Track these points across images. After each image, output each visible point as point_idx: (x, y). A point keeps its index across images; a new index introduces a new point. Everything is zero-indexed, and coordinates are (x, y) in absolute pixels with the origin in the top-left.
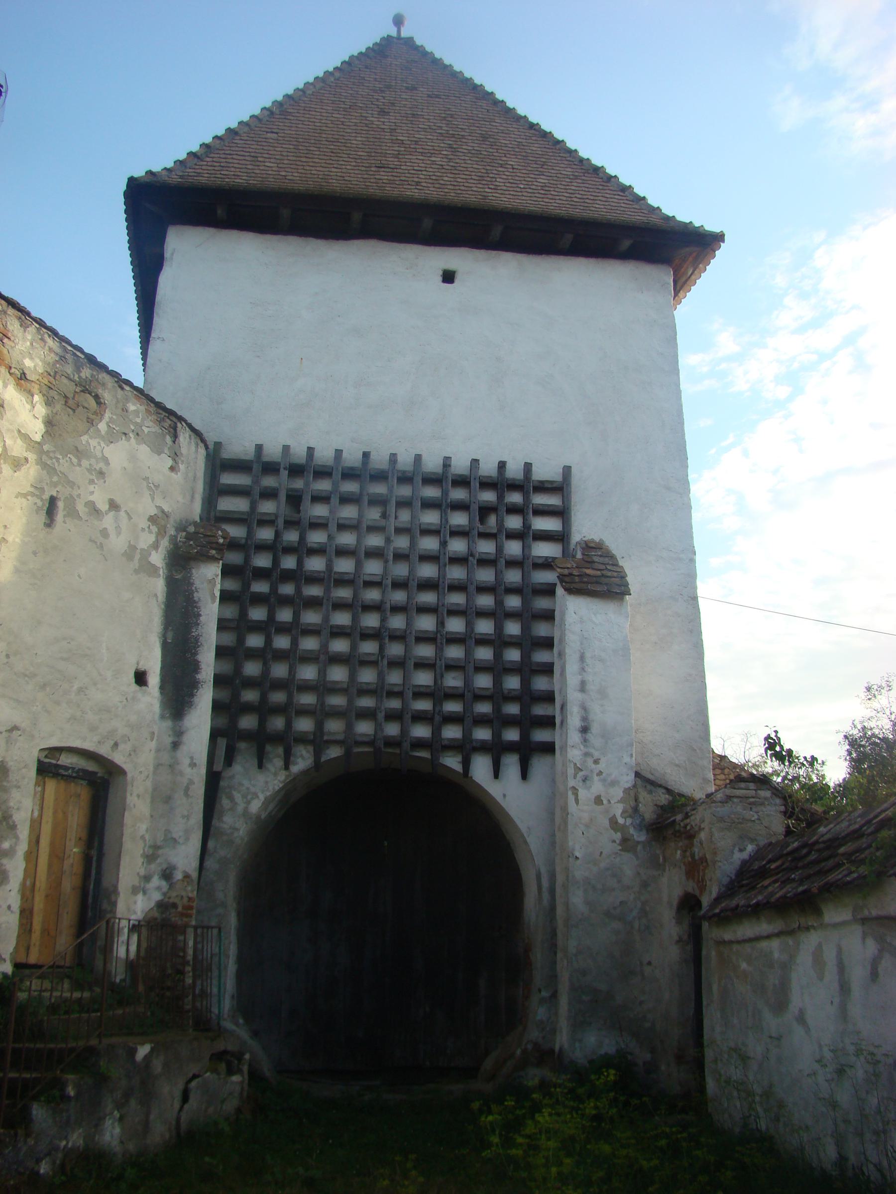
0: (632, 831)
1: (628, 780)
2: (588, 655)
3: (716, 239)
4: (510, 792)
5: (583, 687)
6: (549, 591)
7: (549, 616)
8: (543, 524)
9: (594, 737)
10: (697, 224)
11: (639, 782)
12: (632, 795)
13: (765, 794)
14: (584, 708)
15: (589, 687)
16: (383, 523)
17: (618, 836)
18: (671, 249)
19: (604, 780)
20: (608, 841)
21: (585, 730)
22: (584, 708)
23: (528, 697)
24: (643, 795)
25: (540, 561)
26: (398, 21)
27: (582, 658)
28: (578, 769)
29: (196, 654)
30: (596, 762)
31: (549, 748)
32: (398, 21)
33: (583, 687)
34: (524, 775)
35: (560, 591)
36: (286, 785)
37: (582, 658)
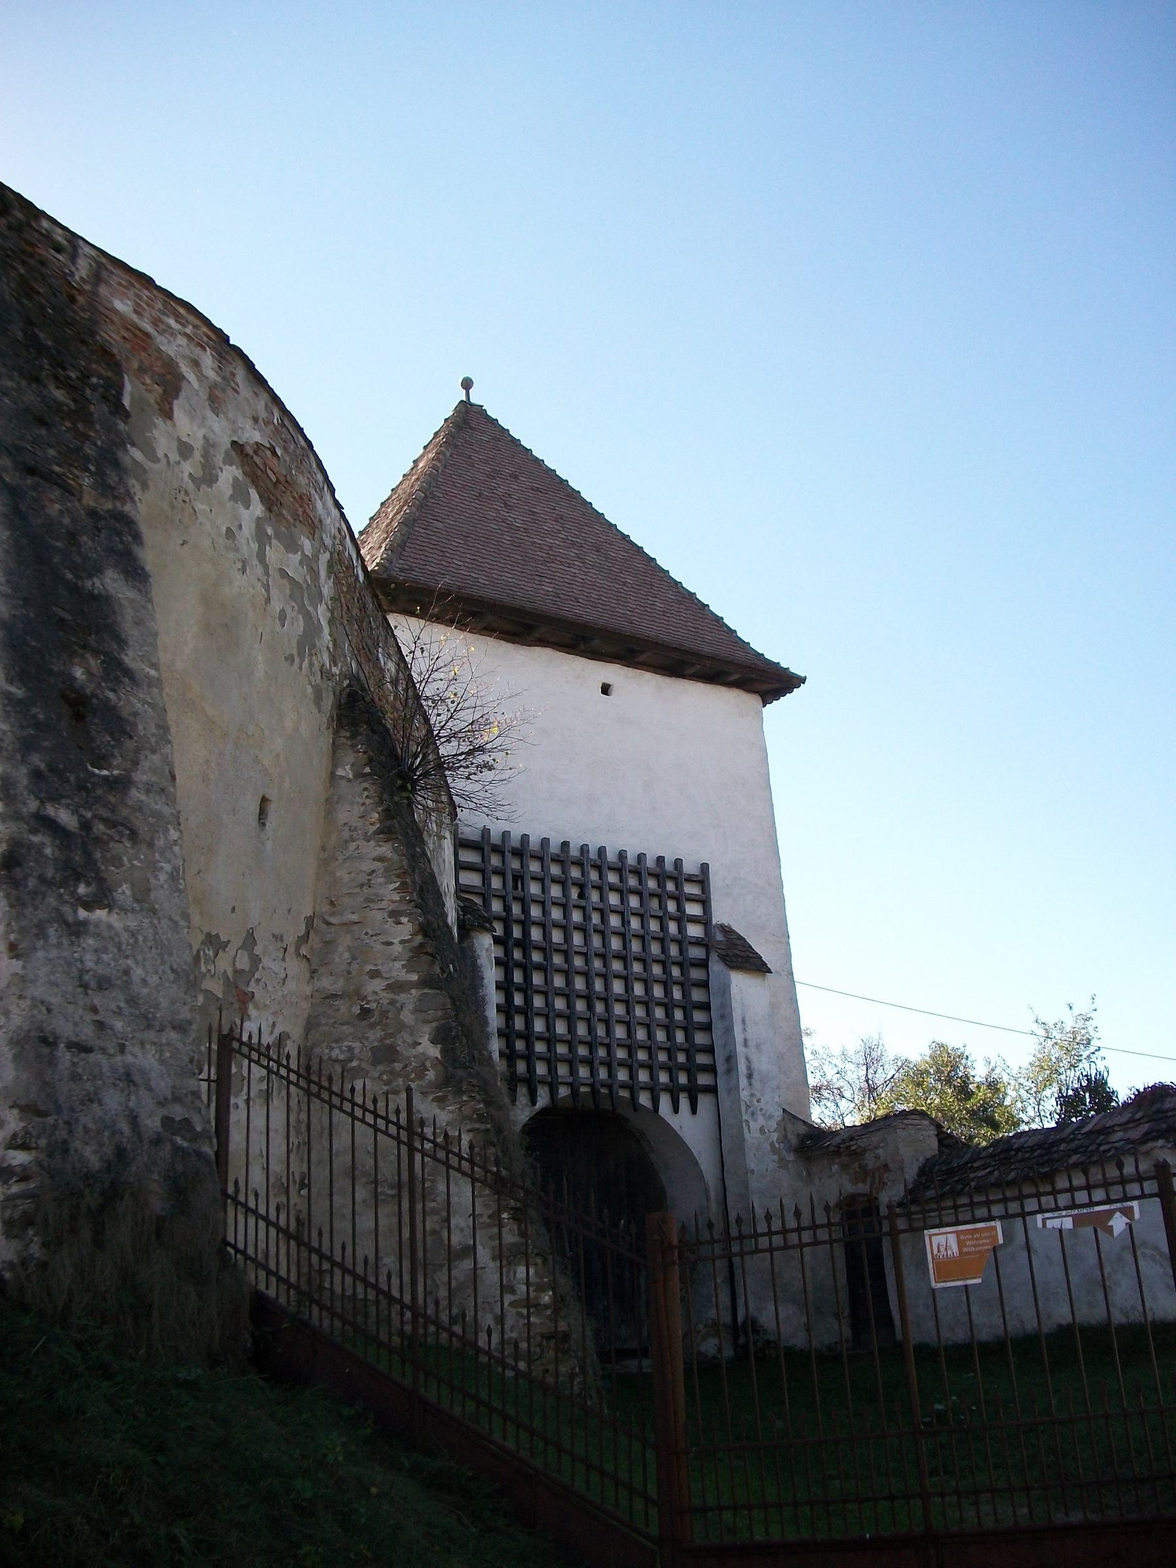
0: (784, 1153)
1: (779, 1114)
2: (747, 1019)
3: (803, 680)
4: (689, 1126)
5: (746, 1043)
6: (703, 964)
7: (704, 985)
8: (693, 909)
9: (756, 1084)
10: (784, 665)
11: (786, 1116)
12: (782, 1127)
13: (926, 1122)
14: (748, 1059)
15: (749, 1043)
16: (582, 903)
17: (776, 1158)
18: (770, 682)
19: (764, 1115)
20: (771, 1162)
21: (750, 1076)
22: (748, 1059)
23: (691, 1050)
24: (790, 1127)
25: (693, 940)
26: (467, 384)
27: (744, 1021)
28: (748, 1107)
29: (484, 1011)
30: (759, 1101)
31: (712, 1090)
32: (467, 384)
33: (746, 1043)
34: (694, 1111)
35: (716, 966)
36: (531, 1119)
37: (744, 1021)
